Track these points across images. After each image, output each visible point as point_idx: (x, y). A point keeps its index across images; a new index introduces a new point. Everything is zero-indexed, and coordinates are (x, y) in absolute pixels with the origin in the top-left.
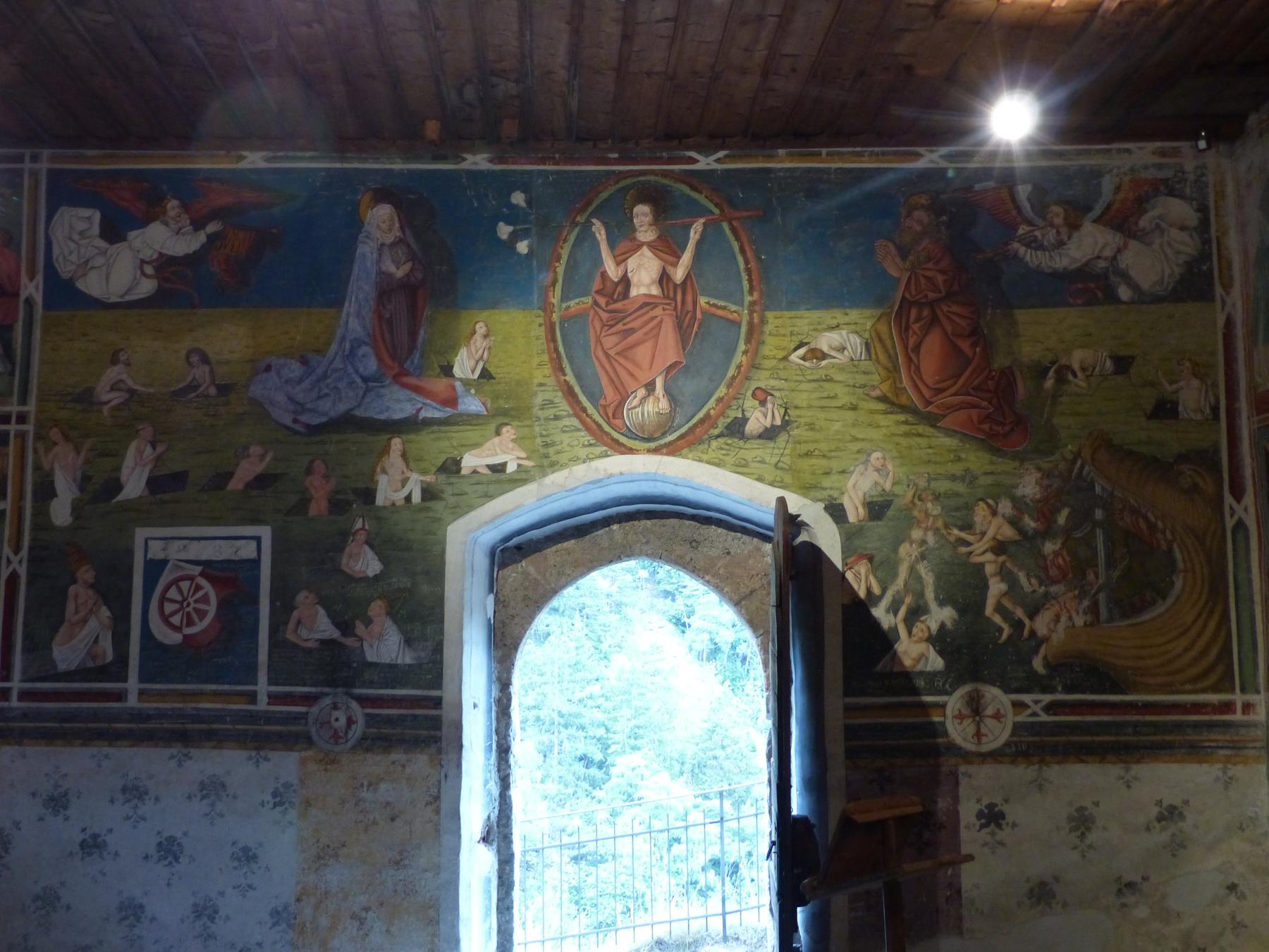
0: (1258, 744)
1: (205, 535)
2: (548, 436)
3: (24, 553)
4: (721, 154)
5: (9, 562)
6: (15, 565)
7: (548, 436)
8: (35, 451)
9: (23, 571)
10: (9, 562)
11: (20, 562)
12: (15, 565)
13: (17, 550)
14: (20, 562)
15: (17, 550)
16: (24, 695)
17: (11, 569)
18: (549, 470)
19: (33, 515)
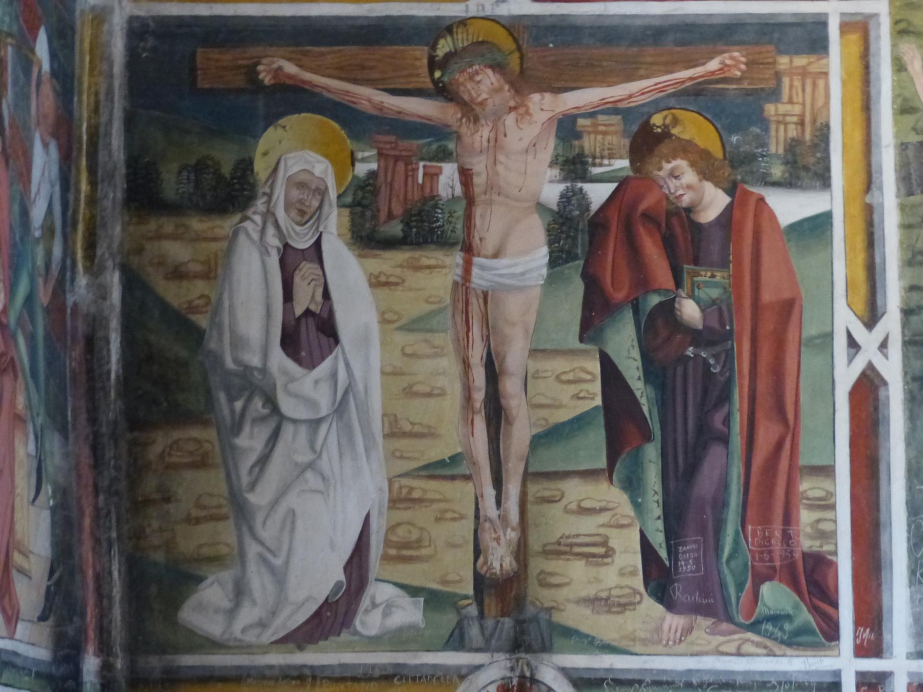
0: (613, 128)
1: (794, 393)
2: (445, 680)
3: (892, 322)
4: (291, 49)
5: (853, 344)
6: (869, 353)
7: (445, 680)
8: (899, 66)
9: (892, 370)
10: (853, 344)
11: (883, 346)
12: (869, 353)
13: (871, 318)
14: (883, 346)
15: (871, 318)
16: (872, 647)
17: (859, 365)
18: (307, 672)
19: (906, 227)
